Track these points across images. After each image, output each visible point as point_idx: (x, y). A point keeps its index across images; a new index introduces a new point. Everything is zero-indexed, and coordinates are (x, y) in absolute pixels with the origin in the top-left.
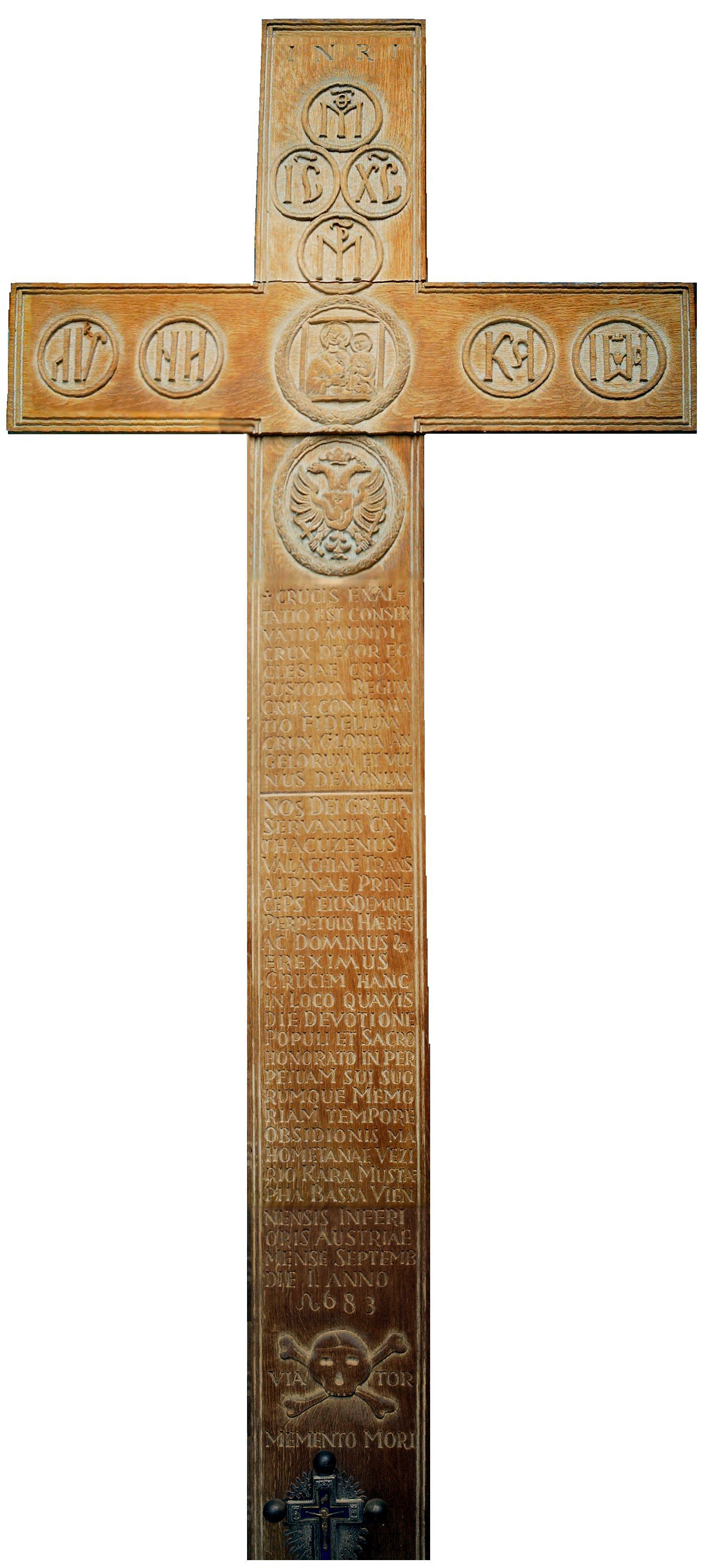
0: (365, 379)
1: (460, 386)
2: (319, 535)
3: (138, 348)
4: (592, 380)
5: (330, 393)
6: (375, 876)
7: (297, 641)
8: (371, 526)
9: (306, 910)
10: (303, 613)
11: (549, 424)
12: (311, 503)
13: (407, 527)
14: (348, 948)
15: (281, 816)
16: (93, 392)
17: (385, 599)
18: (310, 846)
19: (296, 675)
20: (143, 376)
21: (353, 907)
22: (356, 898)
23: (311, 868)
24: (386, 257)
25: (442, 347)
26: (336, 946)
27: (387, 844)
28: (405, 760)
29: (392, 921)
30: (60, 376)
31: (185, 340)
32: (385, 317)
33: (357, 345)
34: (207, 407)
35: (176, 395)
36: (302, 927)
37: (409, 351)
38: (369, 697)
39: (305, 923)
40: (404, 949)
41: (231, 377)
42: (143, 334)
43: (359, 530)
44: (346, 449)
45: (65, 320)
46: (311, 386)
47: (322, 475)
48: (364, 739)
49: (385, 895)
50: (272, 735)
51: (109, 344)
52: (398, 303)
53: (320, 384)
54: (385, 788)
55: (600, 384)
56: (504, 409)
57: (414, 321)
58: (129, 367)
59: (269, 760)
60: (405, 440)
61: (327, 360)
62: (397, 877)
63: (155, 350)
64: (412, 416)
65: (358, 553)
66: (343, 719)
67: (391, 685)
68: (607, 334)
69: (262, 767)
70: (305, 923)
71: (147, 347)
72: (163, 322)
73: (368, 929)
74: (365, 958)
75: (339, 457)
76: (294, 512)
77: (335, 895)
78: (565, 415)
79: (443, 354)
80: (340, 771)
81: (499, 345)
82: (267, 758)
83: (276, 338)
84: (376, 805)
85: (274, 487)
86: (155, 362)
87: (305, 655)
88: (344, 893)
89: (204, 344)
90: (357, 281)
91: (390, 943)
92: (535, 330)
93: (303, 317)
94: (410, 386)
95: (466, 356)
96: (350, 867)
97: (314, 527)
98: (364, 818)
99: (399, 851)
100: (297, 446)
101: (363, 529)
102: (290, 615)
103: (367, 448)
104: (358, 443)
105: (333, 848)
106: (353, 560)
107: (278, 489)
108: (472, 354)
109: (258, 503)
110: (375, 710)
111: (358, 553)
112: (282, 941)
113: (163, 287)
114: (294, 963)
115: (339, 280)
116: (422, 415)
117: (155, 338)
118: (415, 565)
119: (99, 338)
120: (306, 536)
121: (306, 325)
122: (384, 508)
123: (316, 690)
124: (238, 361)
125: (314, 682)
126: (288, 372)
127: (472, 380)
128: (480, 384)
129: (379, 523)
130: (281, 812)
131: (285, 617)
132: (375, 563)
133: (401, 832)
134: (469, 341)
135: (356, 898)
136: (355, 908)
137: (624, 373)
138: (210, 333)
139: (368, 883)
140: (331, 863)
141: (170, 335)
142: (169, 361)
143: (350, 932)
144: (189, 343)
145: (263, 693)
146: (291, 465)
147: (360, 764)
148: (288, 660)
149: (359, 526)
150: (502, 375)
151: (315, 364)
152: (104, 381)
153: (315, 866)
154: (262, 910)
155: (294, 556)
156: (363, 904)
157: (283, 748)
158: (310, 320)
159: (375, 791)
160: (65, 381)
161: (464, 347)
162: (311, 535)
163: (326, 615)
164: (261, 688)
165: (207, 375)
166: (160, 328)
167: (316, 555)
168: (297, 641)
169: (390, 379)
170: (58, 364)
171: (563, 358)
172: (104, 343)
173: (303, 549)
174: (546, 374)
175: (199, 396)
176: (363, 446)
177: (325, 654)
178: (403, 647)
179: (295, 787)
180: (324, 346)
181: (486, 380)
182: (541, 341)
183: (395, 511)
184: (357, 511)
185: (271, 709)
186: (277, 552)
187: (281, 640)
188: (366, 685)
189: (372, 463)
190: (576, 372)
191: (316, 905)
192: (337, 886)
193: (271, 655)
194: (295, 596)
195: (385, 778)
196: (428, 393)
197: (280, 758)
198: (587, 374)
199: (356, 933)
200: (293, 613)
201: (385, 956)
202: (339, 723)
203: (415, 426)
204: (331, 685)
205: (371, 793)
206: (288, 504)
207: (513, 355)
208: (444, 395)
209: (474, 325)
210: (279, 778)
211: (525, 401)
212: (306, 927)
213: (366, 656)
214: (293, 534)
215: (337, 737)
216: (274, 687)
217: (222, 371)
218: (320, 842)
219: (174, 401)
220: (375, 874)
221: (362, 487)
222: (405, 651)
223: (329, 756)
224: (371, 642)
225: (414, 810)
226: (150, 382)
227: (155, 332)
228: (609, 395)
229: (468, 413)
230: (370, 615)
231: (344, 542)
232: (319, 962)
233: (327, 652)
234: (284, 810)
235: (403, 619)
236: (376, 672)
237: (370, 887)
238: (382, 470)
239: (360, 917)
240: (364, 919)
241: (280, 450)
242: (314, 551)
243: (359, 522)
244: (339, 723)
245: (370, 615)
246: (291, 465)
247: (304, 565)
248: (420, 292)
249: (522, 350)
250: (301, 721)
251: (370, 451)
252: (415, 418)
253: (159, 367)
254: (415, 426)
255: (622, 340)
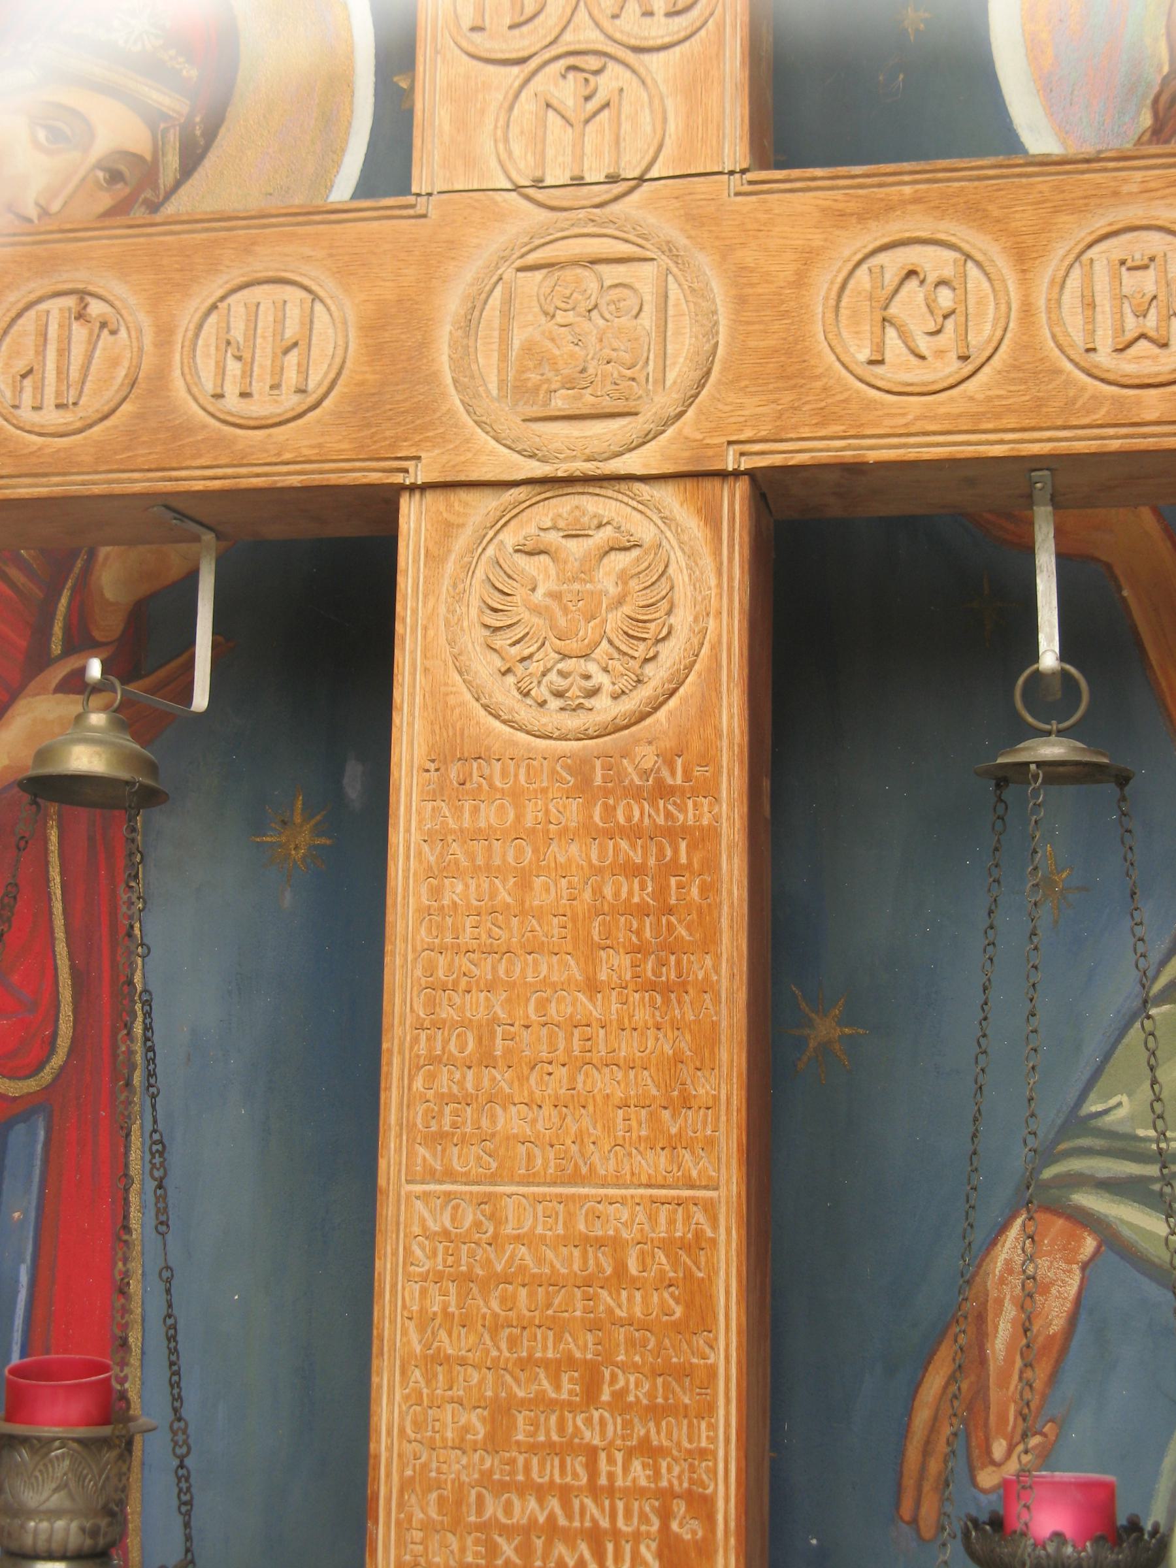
0: (628, 373)
1: (818, 377)
2: (535, 667)
3: (179, 338)
4: (1088, 350)
5: (560, 403)
6: (637, 1368)
7: (488, 867)
8: (642, 646)
9: (491, 1436)
10: (502, 806)
11: (1001, 442)
12: (522, 609)
13: (716, 647)
14: (577, 1524)
15: (446, 1233)
16: (91, 426)
17: (670, 781)
18: (503, 1300)
19: (484, 936)
20: (189, 391)
21: (587, 1434)
22: (596, 1414)
23: (504, 1345)
24: (671, 127)
25: (783, 302)
26: (551, 1518)
27: (662, 1301)
28: (705, 1123)
29: (669, 1469)
30: (27, 399)
31: (271, 319)
32: (669, 249)
33: (612, 307)
34: (314, 442)
35: (252, 423)
36: (482, 1473)
37: (715, 312)
38: (631, 986)
39: (488, 1464)
40: (694, 1533)
41: (362, 383)
42: (188, 312)
43: (616, 655)
44: (593, 505)
45: (38, 294)
46: (520, 390)
47: (542, 557)
48: (619, 1075)
49: (655, 1412)
50: (434, 1060)
51: (123, 333)
52: (694, 219)
53: (537, 389)
54: (660, 1181)
55: (1104, 358)
56: (910, 417)
57: (724, 253)
58: (161, 376)
59: (426, 1112)
60: (708, 485)
61: (553, 340)
62: (683, 1373)
63: (213, 340)
64: (724, 439)
65: (615, 697)
66: (576, 1032)
67: (678, 963)
68: (1117, 255)
69: (412, 1127)
70: (488, 1464)
71: (197, 335)
72: (229, 286)
73: (619, 1483)
74: (610, 1547)
75: (577, 520)
76: (486, 626)
77: (552, 1405)
78: (1033, 423)
79: (785, 314)
80: (569, 1142)
81: (896, 291)
82: (420, 1109)
83: (451, 304)
84: (641, 1217)
85: (446, 583)
86: (212, 363)
87: (504, 896)
88: (570, 1403)
89: (309, 322)
90: (613, 179)
91: (665, 1516)
92: (968, 256)
93: (505, 259)
94: (719, 382)
95: (830, 315)
96: (584, 1347)
97: (526, 653)
98: (616, 1245)
99: (687, 1316)
100: (494, 504)
101: (625, 654)
102: (476, 810)
103: (634, 504)
104: (615, 495)
105: (549, 1306)
106: (605, 708)
107: (455, 586)
108: (843, 311)
109: (415, 611)
110: (642, 1016)
111: (615, 697)
112: (441, 1500)
113: (230, 219)
114: (463, 1550)
115: (578, 182)
116: (742, 437)
117: (213, 318)
118: (731, 717)
119: (103, 325)
120: (509, 671)
121: (509, 274)
122: (669, 613)
123: (523, 970)
124: (376, 351)
125: (520, 952)
126: (474, 367)
127: (843, 365)
128: (859, 371)
129: (658, 641)
130: (448, 1224)
131: (467, 815)
132: (649, 714)
133: (692, 1275)
134: (836, 287)
135: (596, 1414)
136: (591, 1437)
137: (1152, 334)
138: (322, 301)
139: (621, 1383)
140: (545, 1338)
141: (242, 310)
142: (239, 358)
143: (580, 1488)
144: (280, 322)
145: (418, 972)
146: (481, 542)
147: (609, 1128)
148: (468, 906)
149: (618, 649)
150: (905, 350)
151: (529, 349)
152: (112, 405)
153: (513, 1343)
154: (402, 1431)
155: (485, 707)
156: (610, 1429)
157: (455, 1089)
158: (519, 263)
159: (640, 1185)
160: (37, 408)
161: (826, 298)
162: (520, 669)
163: (547, 812)
164: (415, 960)
165: (316, 378)
166: (223, 298)
167: (529, 701)
168: (488, 867)
169: (679, 371)
170: (24, 376)
171: (1027, 310)
172: (113, 333)
173: (504, 693)
174: (994, 344)
175: (300, 422)
176: (626, 499)
177: (543, 893)
178: (703, 882)
179: (477, 1171)
180: (546, 314)
181: (871, 362)
182: (983, 279)
183: (690, 619)
184: (615, 621)
185: (431, 1003)
186: (452, 700)
187: (457, 862)
188: (627, 960)
189: (645, 531)
190: (1054, 337)
191: (513, 1426)
192: (558, 1388)
193: (436, 893)
194: (487, 772)
195: (663, 1159)
196: (753, 394)
197: (447, 1110)
198: (1078, 338)
199: (593, 1490)
200: (482, 806)
201: (654, 1546)
202: (569, 1038)
203: (730, 458)
204: (555, 959)
205: (632, 1191)
206: (474, 612)
207: (924, 309)
208: (787, 398)
209: (847, 253)
210: (444, 1151)
211: (952, 399)
212: (491, 1472)
213: (628, 899)
214: (484, 666)
215: (564, 1070)
216: (442, 961)
217: (346, 372)
218: (523, 1293)
219: (250, 432)
220: (635, 1365)
221: (623, 577)
222: (705, 890)
223: (547, 1110)
224: (635, 871)
225: (722, 1230)
226: (201, 401)
227: (214, 307)
228: (1125, 381)
229: (837, 429)
230: (637, 814)
231: (587, 677)
232: (516, 1550)
233: (548, 890)
234: (453, 1219)
235: (705, 822)
236: (648, 934)
237: (624, 1391)
238: (664, 543)
239: (603, 1456)
240: (611, 1460)
241: (459, 514)
242: (527, 694)
243: (617, 643)
244: (569, 1038)
245: (637, 814)
246: (481, 542)
247: (504, 722)
248: (737, 194)
249: (945, 298)
250: (493, 1034)
251: (640, 507)
252: (730, 443)
253: (221, 371)
254: (730, 458)
255: (1146, 267)
